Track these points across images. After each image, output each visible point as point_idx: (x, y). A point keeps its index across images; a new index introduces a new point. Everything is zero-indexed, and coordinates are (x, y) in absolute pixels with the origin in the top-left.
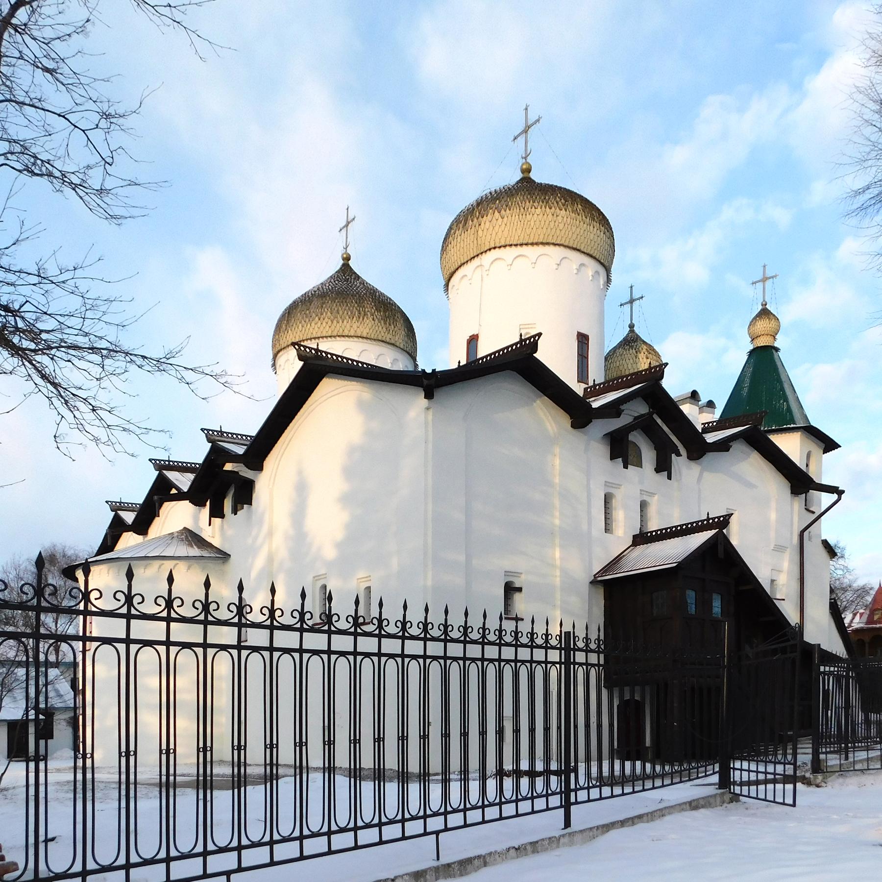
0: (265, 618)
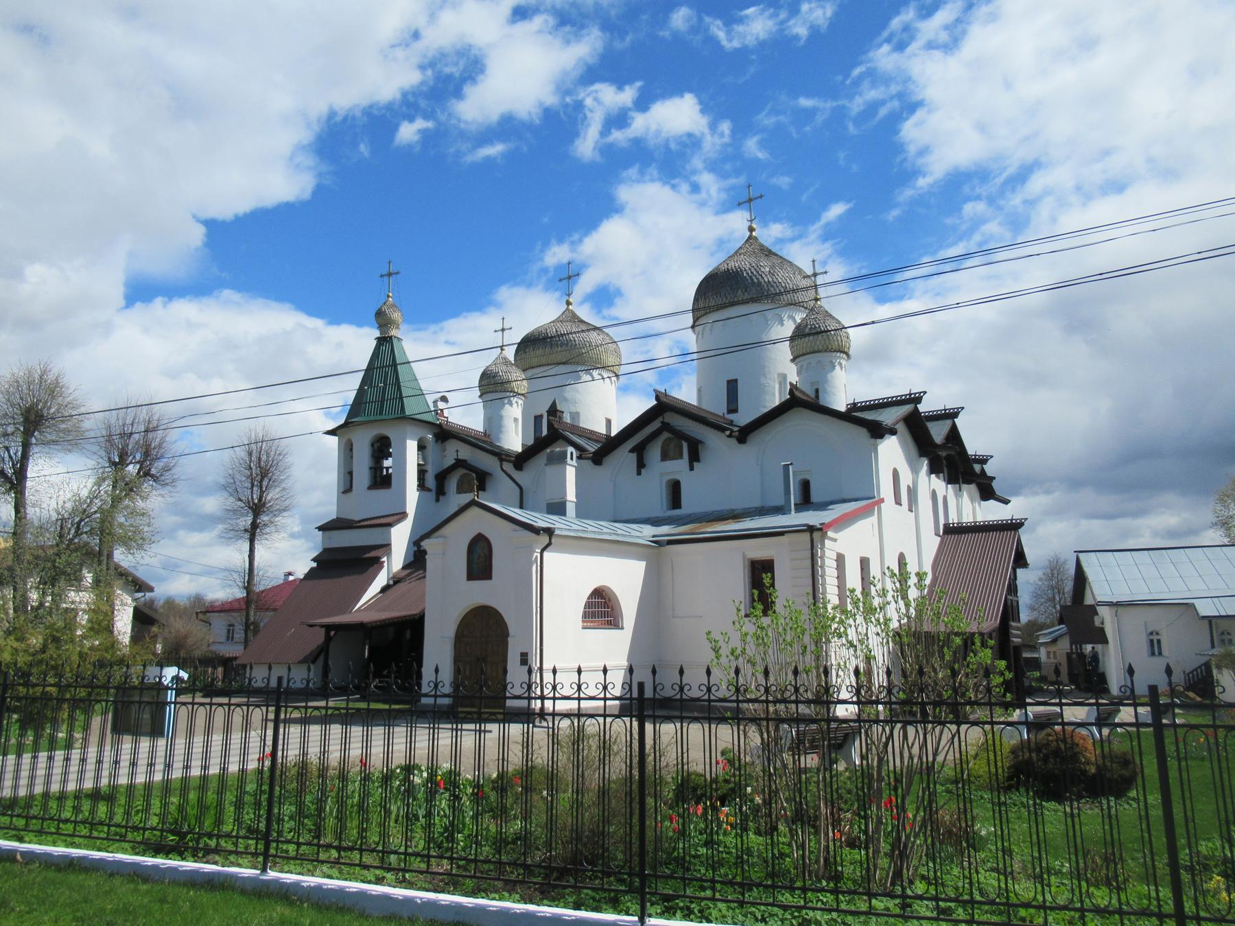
0: (703, 693)
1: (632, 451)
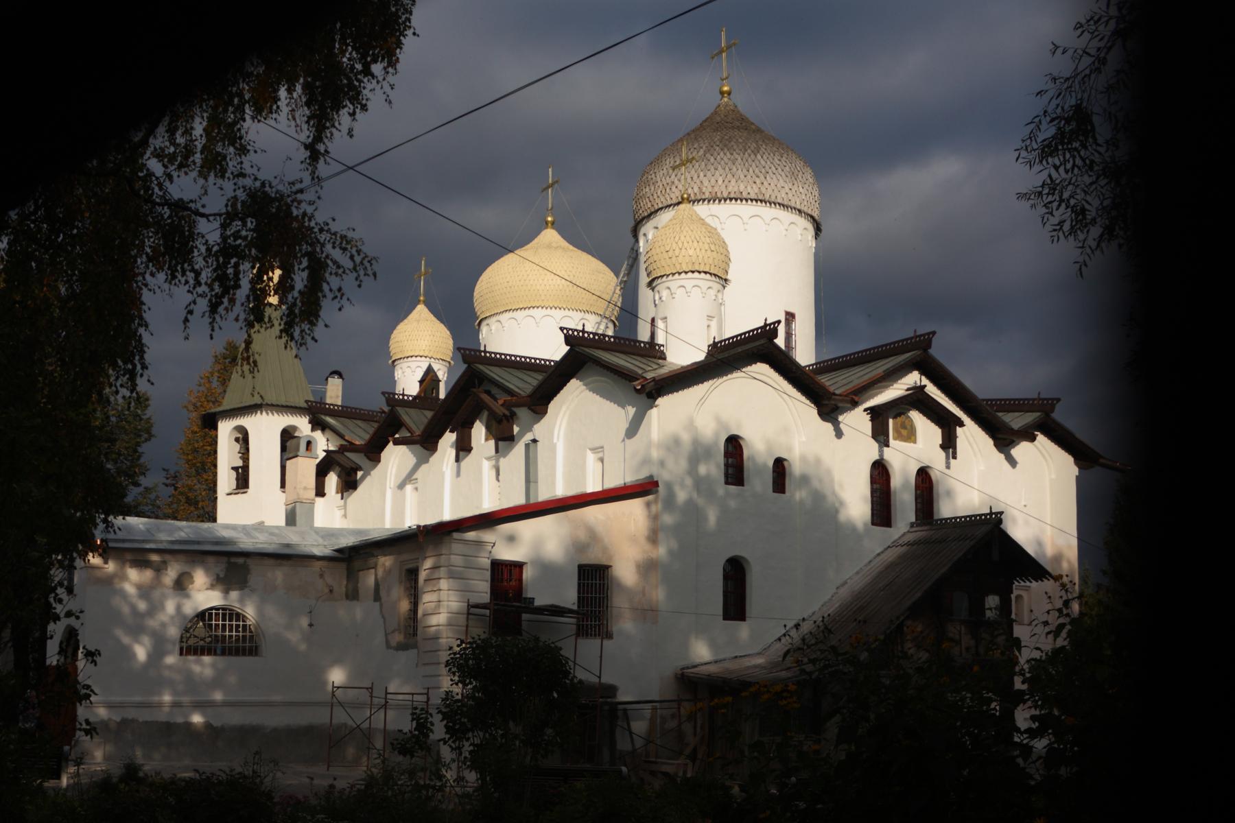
1: (452, 431)
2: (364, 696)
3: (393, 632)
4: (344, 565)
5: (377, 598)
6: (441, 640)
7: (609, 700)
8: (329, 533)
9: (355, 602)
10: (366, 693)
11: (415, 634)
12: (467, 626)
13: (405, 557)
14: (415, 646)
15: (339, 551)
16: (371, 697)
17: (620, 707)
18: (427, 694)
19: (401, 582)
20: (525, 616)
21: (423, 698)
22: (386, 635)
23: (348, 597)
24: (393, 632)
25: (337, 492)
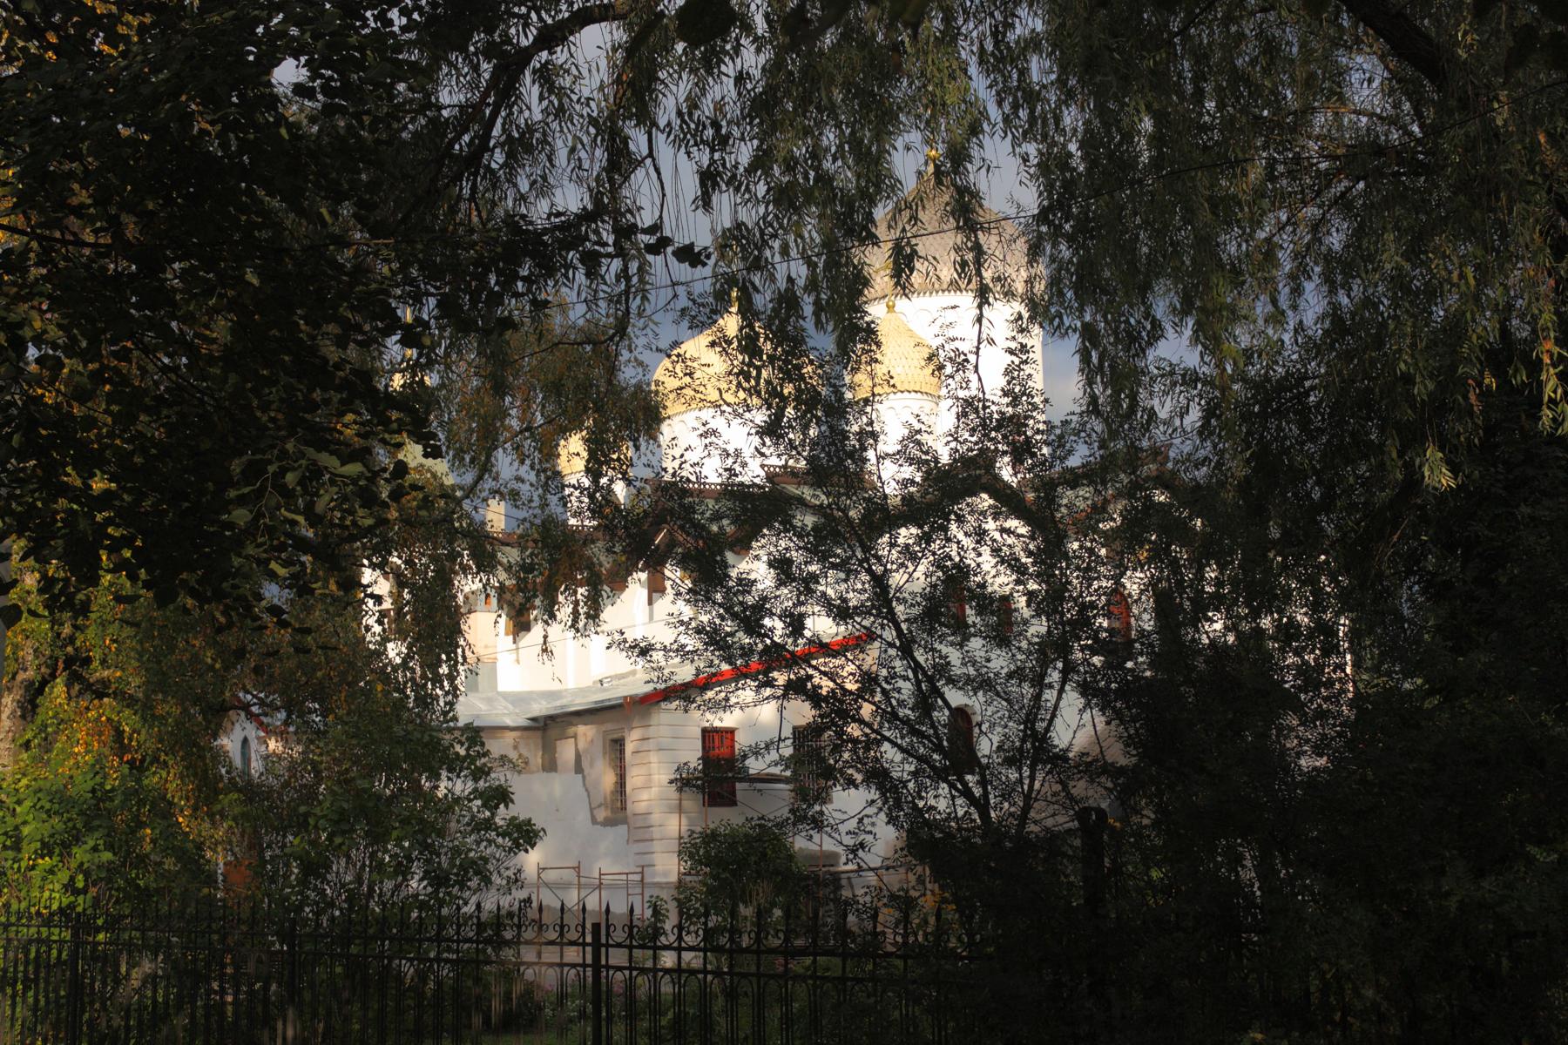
2: (570, 875)
3: (599, 806)
4: (539, 734)
5: (579, 768)
6: (653, 816)
7: (832, 869)
8: (518, 699)
9: (553, 774)
10: (573, 873)
11: (624, 808)
12: (680, 800)
13: (609, 726)
14: (624, 821)
15: (533, 719)
16: (579, 877)
17: (843, 876)
18: (642, 873)
19: (605, 753)
20: (738, 786)
21: (637, 877)
22: (592, 810)
23: (544, 769)
24: (599, 806)
25: (507, 634)
